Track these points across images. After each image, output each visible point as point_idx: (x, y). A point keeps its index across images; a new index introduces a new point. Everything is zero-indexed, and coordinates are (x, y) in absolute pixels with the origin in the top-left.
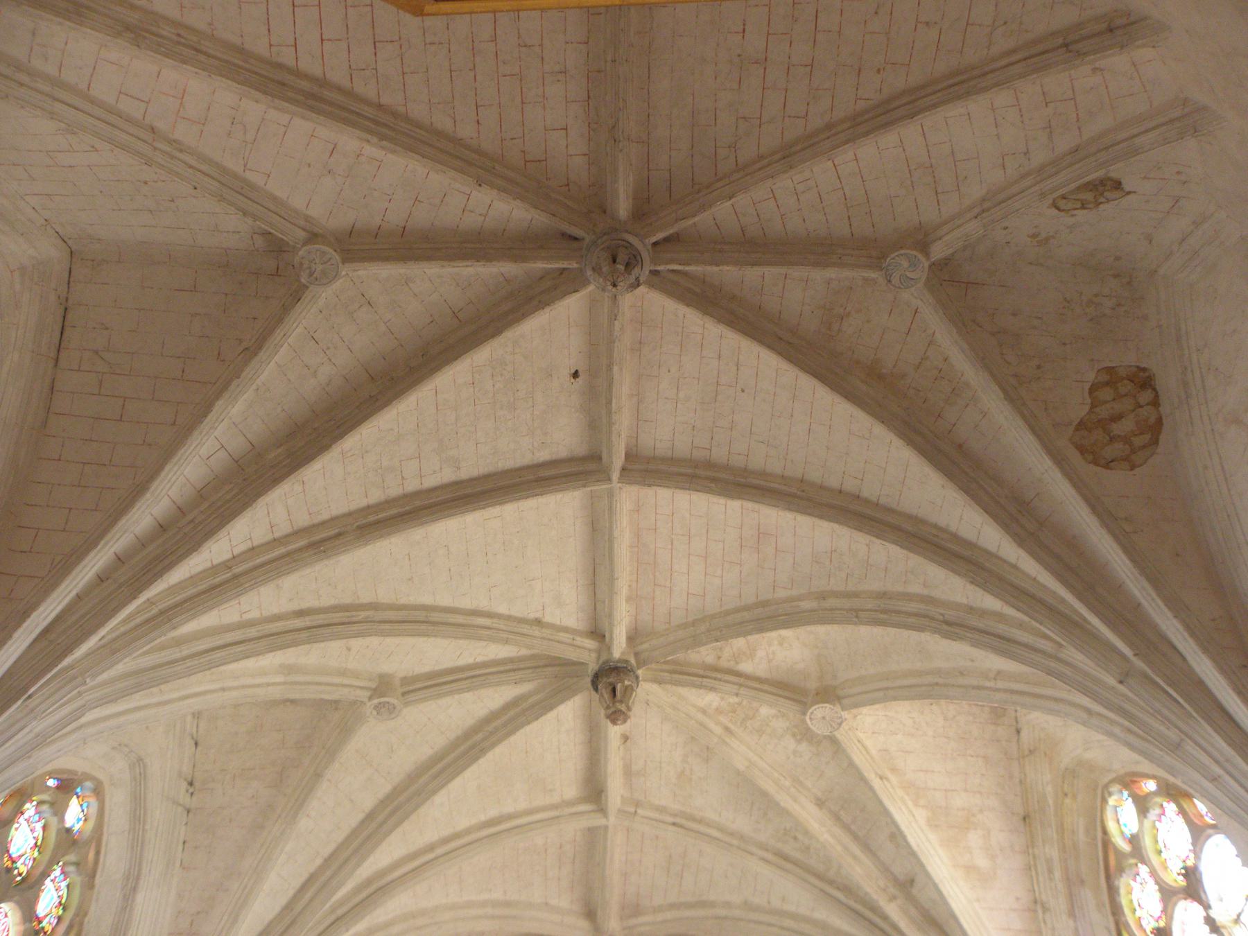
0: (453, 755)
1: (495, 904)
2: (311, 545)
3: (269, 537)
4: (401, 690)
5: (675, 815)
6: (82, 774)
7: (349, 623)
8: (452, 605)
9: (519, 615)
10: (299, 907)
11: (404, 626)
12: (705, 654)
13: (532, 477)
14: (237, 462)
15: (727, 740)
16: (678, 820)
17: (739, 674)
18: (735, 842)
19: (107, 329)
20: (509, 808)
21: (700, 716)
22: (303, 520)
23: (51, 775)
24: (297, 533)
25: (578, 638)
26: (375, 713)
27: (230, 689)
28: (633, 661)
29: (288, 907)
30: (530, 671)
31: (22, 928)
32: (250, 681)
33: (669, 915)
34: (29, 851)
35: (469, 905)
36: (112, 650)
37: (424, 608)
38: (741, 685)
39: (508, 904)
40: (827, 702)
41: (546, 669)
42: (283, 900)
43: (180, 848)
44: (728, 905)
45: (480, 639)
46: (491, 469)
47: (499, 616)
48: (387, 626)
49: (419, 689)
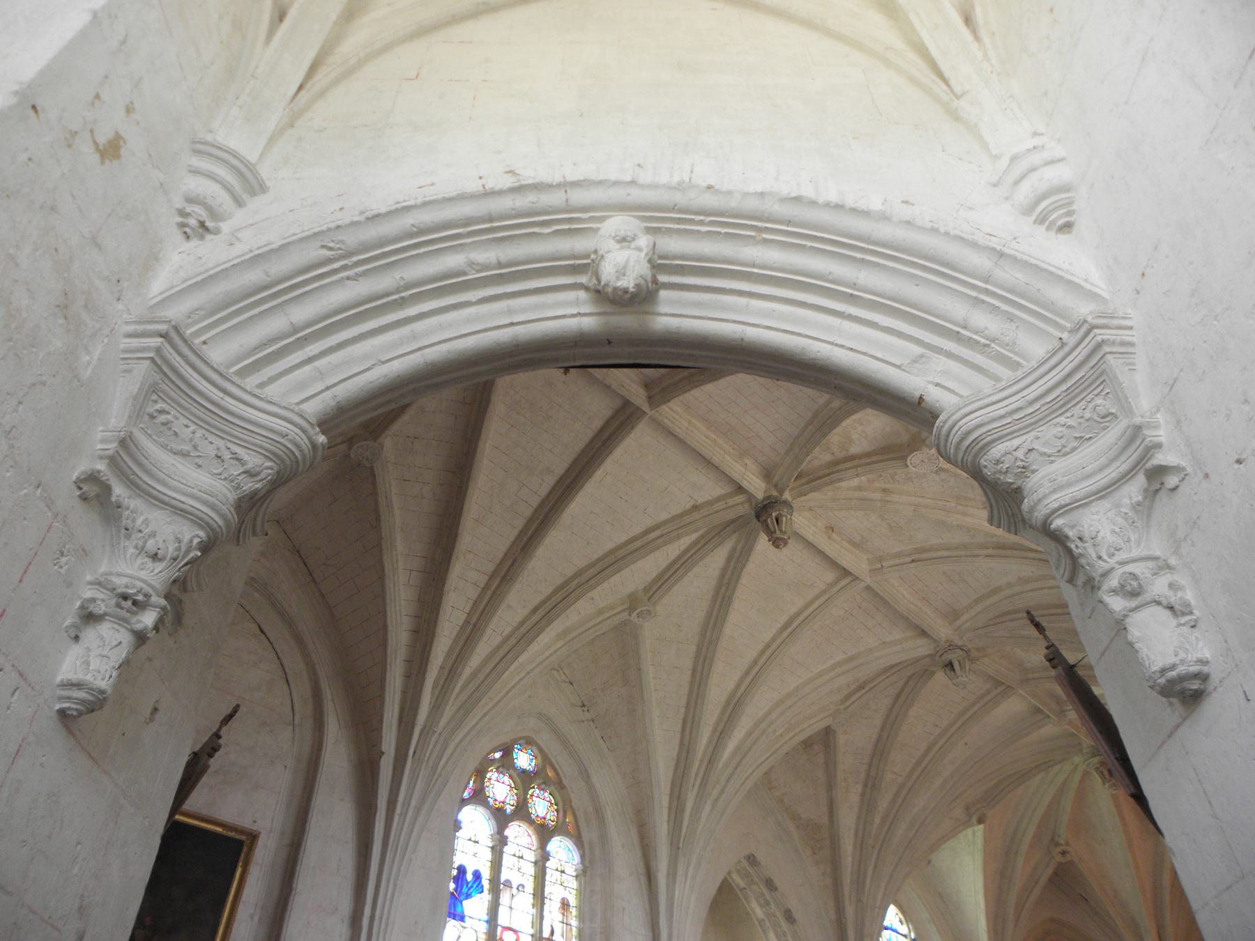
0: (716, 609)
1: (840, 664)
2: (504, 578)
3: (479, 590)
4: (646, 598)
5: (910, 555)
6: (511, 740)
7: (569, 595)
8: (629, 537)
9: (679, 512)
10: (686, 743)
11: (604, 573)
12: (820, 457)
13: (600, 444)
14: (424, 572)
15: (888, 498)
16: (913, 557)
17: (852, 458)
18: (962, 553)
19: (320, 548)
20: (793, 610)
21: (858, 494)
22: (490, 568)
23: (494, 751)
24: (492, 576)
25: (730, 500)
26: (640, 619)
27: (532, 670)
28: (775, 493)
29: (681, 744)
30: (717, 538)
31: (532, 828)
32: (541, 658)
33: (978, 608)
34: (509, 792)
35: (821, 674)
36: (437, 708)
37: (612, 552)
38: (857, 467)
39: (851, 659)
40: (915, 451)
41: (726, 530)
42: (677, 741)
43: (602, 742)
44: (1009, 585)
45: (658, 548)
46: (573, 456)
47: (664, 523)
48: (592, 581)
49: (657, 591)
